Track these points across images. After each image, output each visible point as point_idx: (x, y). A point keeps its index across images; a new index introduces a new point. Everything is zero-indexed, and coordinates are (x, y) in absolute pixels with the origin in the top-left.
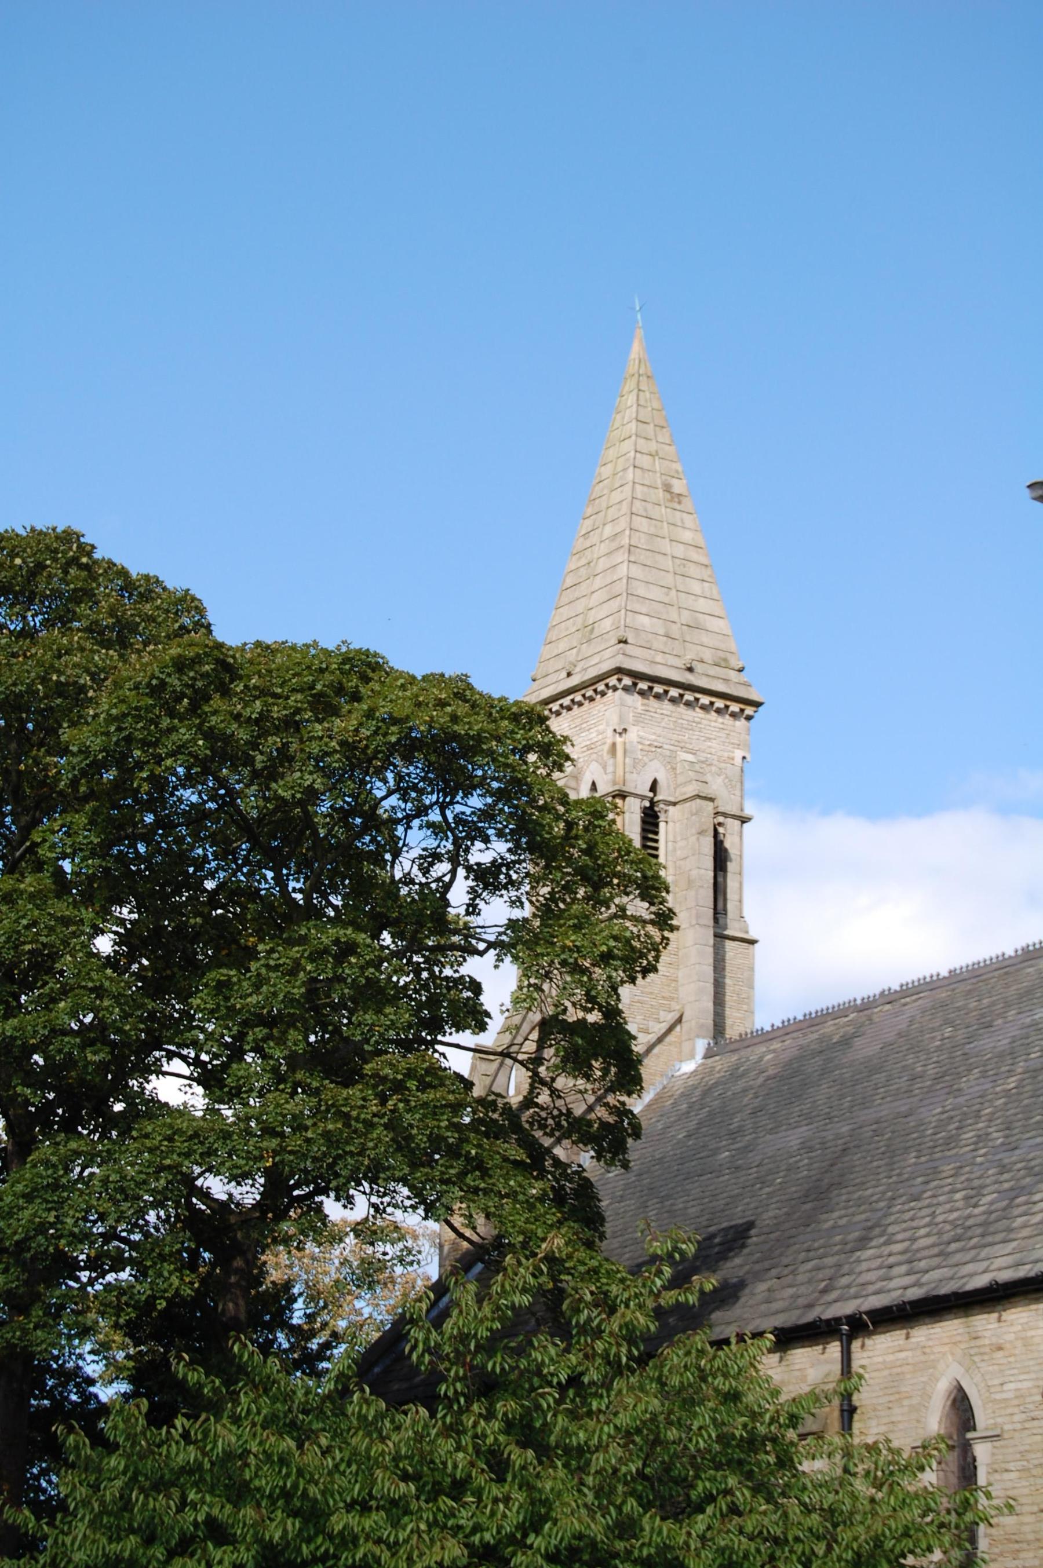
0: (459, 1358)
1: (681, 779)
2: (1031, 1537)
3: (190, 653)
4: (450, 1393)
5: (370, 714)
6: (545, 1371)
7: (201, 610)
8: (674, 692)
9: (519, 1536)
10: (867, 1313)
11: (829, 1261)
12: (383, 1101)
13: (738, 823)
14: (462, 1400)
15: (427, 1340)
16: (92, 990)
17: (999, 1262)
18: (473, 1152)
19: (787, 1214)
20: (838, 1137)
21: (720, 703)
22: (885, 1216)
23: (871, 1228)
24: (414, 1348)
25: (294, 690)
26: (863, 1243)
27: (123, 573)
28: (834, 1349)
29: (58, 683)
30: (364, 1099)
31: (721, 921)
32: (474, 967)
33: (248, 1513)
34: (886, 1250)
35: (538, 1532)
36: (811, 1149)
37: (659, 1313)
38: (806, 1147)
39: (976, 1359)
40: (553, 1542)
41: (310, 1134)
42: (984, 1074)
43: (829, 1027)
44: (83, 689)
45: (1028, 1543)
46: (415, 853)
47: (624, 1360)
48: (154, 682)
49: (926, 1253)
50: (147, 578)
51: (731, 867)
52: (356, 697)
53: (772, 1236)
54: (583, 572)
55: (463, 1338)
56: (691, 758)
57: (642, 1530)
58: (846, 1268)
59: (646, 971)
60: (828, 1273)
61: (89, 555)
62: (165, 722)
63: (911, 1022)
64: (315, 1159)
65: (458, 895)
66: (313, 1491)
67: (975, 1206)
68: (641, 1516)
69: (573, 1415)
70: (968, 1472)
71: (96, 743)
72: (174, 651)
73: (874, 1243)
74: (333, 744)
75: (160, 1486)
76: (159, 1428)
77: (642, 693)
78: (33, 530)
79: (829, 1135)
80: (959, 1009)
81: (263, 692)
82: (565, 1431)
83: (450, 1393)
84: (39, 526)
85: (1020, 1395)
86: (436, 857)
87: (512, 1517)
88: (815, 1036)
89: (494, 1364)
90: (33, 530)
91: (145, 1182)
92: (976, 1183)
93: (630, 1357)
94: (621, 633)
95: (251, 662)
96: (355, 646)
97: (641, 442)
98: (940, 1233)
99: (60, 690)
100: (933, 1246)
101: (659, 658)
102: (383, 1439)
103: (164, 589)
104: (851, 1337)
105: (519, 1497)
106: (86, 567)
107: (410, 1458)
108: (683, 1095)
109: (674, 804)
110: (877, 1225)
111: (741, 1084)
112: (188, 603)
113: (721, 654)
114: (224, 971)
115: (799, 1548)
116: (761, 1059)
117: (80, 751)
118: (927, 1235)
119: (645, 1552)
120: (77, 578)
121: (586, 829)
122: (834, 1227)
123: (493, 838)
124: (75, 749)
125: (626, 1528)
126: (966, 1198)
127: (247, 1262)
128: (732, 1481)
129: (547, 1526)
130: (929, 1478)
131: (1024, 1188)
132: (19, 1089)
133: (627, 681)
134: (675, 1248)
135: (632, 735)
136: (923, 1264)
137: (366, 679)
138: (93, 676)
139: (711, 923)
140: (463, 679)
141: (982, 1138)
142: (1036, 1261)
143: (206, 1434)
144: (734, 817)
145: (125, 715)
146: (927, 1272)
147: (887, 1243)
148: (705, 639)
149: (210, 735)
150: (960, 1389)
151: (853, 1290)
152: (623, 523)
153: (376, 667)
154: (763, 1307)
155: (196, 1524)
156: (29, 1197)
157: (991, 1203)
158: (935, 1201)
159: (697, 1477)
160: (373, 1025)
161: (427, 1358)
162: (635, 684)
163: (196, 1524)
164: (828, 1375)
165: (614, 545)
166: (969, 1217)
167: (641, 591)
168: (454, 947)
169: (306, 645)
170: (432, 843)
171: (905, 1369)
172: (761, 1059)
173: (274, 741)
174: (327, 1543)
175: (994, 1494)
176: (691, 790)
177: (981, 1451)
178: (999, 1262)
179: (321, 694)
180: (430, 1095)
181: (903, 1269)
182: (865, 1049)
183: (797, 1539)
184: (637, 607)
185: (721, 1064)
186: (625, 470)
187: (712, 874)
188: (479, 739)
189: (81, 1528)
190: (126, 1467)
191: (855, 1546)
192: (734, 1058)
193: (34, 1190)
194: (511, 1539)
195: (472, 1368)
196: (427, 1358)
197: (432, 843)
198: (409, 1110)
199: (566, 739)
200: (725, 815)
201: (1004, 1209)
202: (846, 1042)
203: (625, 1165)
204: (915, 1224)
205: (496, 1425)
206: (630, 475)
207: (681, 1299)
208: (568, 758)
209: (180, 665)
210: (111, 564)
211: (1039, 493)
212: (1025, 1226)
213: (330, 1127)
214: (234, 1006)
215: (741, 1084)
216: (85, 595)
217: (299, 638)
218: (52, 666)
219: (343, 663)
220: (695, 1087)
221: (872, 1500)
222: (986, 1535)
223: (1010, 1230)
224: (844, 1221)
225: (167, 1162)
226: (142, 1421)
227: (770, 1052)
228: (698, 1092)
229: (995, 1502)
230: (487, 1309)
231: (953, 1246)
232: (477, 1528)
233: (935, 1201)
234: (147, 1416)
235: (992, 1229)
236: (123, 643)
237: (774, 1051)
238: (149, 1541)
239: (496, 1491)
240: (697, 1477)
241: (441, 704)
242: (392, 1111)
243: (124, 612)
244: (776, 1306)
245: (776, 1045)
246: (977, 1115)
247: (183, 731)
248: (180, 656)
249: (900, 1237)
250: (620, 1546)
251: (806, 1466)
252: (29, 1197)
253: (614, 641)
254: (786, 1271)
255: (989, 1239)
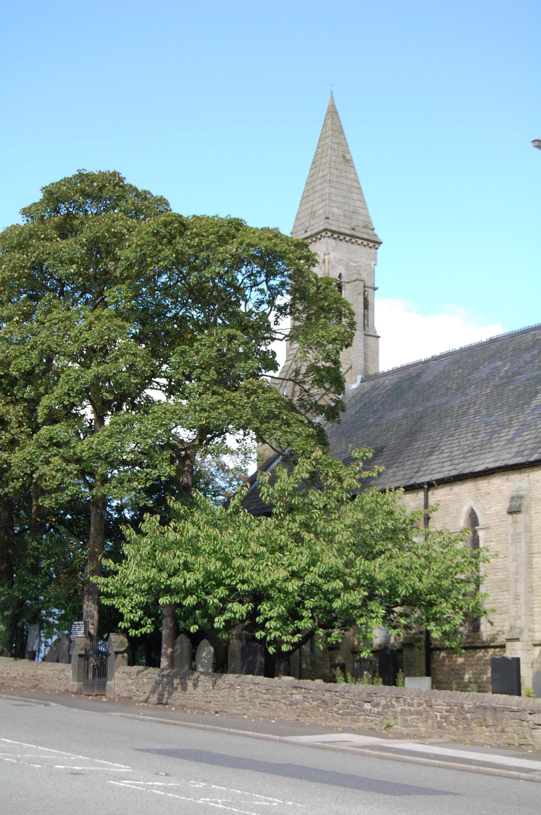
0: (280, 499)
1: (350, 273)
2: (501, 567)
3: (169, 219)
4: (278, 512)
5: (241, 243)
6: (314, 503)
7: (167, 204)
8: (348, 238)
9: (307, 567)
10: (435, 480)
11: (418, 461)
12: (249, 398)
13: (372, 290)
14: (282, 515)
15: (268, 491)
16: (132, 354)
17: (488, 461)
18: (285, 417)
19: (399, 443)
20: (418, 412)
21: (365, 243)
22: (439, 443)
23: (434, 448)
24: (263, 495)
25: (211, 234)
26: (431, 453)
27: (136, 189)
28: (421, 494)
29: (114, 232)
30: (241, 397)
31: (367, 329)
32: (274, 346)
33: (201, 559)
34: (441, 456)
35: (314, 565)
36: (407, 417)
37: (361, 480)
38: (405, 416)
39: (479, 498)
40: (321, 570)
41: (220, 411)
42: (476, 388)
43: (411, 370)
44: (124, 235)
45: (500, 569)
46: (253, 301)
47: (345, 499)
48: (155, 231)
49: (457, 457)
50: (145, 191)
51: (370, 307)
52: (234, 237)
53: (394, 451)
54: (311, 191)
55: (283, 490)
56: (354, 264)
57: (356, 564)
58: (425, 463)
59: (347, 346)
60: (417, 465)
61: (123, 182)
62: (160, 247)
63: (445, 367)
64: (223, 421)
65: (271, 318)
66: (227, 550)
67: (476, 439)
68: (355, 559)
69: (326, 521)
70: (475, 542)
71: (132, 256)
72: (163, 218)
73: (436, 453)
74: (227, 255)
75: (165, 549)
76: (164, 526)
77: (335, 239)
78: (100, 172)
79: (414, 412)
80: (464, 362)
81: (197, 235)
82: (324, 527)
83: (278, 512)
84: (103, 170)
85: (497, 512)
86: (262, 302)
87: (304, 560)
88: (406, 373)
89: (295, 501)
90: (100, 172)
91: (155, 431)
92: (476, 430)
93: (347, 498)
94: (327, 215)
95: (193, 223)
96: (233, 216)
97: (333, 139)
98: (463, 449)
99: (115, 235)
100: (460, 454)
101: (342, 225)
102: (253, 530)
103: (152, 196)
104: (428, 490)
105: (306, 552)
106: (121, 187)
107: (263, 537)
108: (352, 397)
109: (348, 283)
110: (436, 446)
111: (376, 393)
112: (162, 201)
113: (365, 223)
114: (184, 347)
115: (417, 571)
116: (384, 383)
117: (125, 259)
118: (457, 450)
119: (358, 573)
120: (119, 191)
121: (324, 290)
122: (419, 447)
123: (285, 294)
124: (123, 258)
125: (349, 564)
126: (473, 436)
127: (191, 462)
128: (390, 546)
129: (319, 563)
130: (460, 545)
131: (496, 431)
132: (104, 394)
133: (329, 234)
134: (364, 455)
135: (332, 255)
136: (456, 461)
137: (238, 230)
138: (128, 230)
139: (363, 329)
140: (277, 229)
141: (477, 412)
142: (503, 460)
143: (184, 528)
144: (371, 288)
145: (143, 244)
146: (458, 464)
147: (441, 453)
148: (360, 217)
149: (177, 252)
150: (472, 510)
151: (428, 472)
152: (326, 171)
153: (241, 225)
154: (392, 479)
155: (179, 564)
156: (110, 437)
157: (483, 437)
158: (460, 437)
159: (376, 544)
160: (244, 368)
161: (268, 498)
162: (332, 235)
163: (179, 564)
164: (419, 505)
165: (323, 180)
166: (474, 443)
167: (334, 198)
168: (267, 338)
169: (214, 217)
170: (260, 297)
171: (450, 502)
172: (384, 383)
173: (203, 254)
174: (232, 571)
175: (490, 550)
176: (354, 277)
177: (481, 534)
178: (488, 461)
179: (221, 236)
180: (267, 395)
181: (449, 463)
182: (426, 378)
183: (416, 568)
184: (333, 204)
185: (367, 385)
186: (327, 150)
187: (363, 310)
188: (285, 252)
189: (132, 564)
190: (151, 542)
191: (440, 570)
192: (373, 382)
193: (112, 434)
194: (304, 569)
195: (286, 503)
196: (268, 498)
197: (260, 297)
198: (260, 401)
199: (315, 254)
200: (368, 287)
201: (489, 440)
202: (419, 376)
203: (339, 422)
204: (452, 446)
205: (297, 525)
206: (329, 152)
207: (371, 475)
208: (317, 262)
209: (165, 224)
210: (131, 186)
211: (537, 144)
212: (498, 446)
213: (229, 408)
214: (188, 361)
215: (376, 393)
216: (121, 197)
217: (210, 213)
218: (111, 225)
219: (229, 223)
220: (357, 394)
221: (442, 553)
222: (483, 566)
223: (491, 448)
224: (422, 445)
225: (164, 422)
226: (157, 524)
227: (387, 380)
228: (359, 396)
229: (491, 553)
230: (292, 480)
231: (469, 454)
232: (290, 565)
233: (460, 437)
234: (160, 522)
235: (484, 447)
236: (136, 216)
237: (389, 379)
238: (160, 571)
239: (297, 550)
240: (376, 544)
241: (270, 239)
242: (253, 401)
243: (138, 204)
244: (396, 478)
245: (390, 377)
246: (475, 403)
247: (167, 250)
248: (165, 220)
249: (446, 451)
250: (347, 571)
251: (415, 539)
252: (110, 437)
253: (324, 218)
254: (400, 464)
255: (483, 451)
